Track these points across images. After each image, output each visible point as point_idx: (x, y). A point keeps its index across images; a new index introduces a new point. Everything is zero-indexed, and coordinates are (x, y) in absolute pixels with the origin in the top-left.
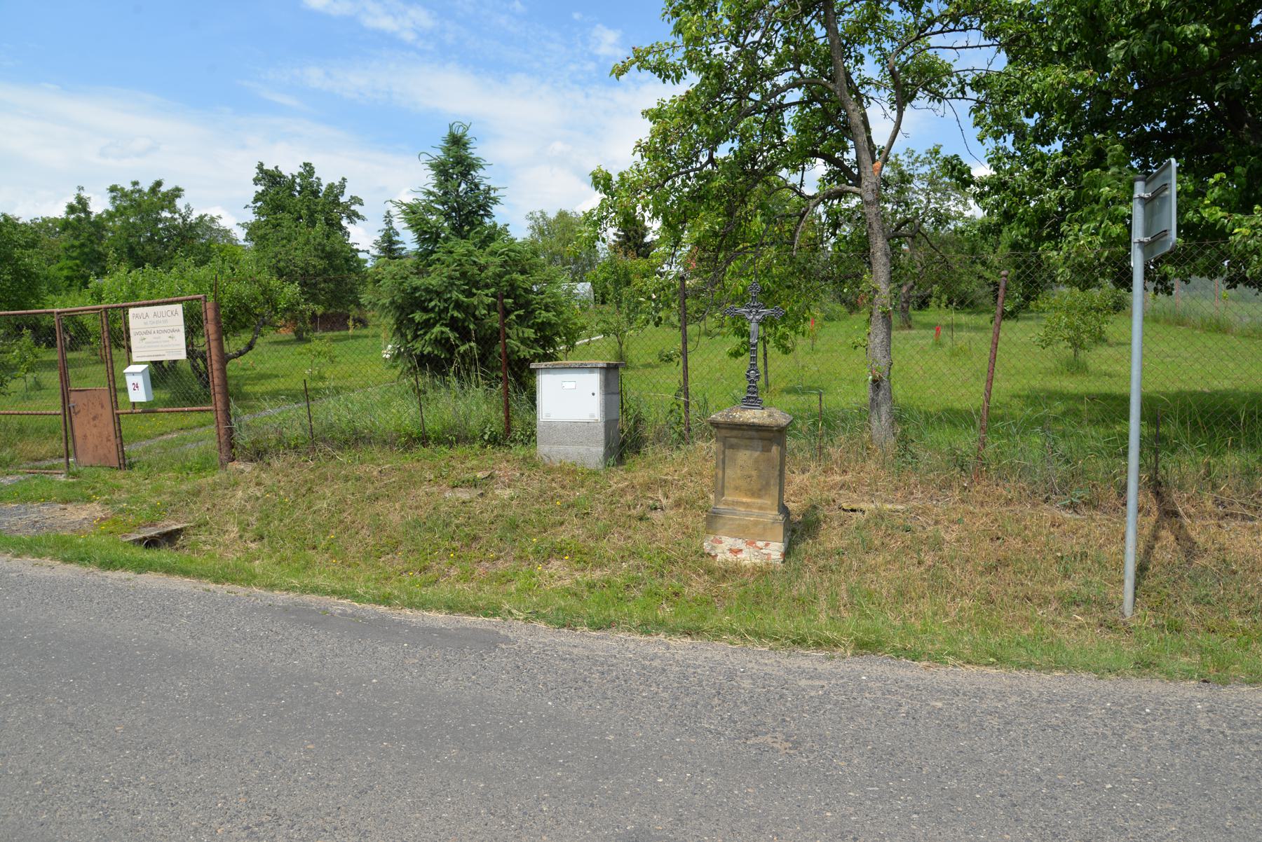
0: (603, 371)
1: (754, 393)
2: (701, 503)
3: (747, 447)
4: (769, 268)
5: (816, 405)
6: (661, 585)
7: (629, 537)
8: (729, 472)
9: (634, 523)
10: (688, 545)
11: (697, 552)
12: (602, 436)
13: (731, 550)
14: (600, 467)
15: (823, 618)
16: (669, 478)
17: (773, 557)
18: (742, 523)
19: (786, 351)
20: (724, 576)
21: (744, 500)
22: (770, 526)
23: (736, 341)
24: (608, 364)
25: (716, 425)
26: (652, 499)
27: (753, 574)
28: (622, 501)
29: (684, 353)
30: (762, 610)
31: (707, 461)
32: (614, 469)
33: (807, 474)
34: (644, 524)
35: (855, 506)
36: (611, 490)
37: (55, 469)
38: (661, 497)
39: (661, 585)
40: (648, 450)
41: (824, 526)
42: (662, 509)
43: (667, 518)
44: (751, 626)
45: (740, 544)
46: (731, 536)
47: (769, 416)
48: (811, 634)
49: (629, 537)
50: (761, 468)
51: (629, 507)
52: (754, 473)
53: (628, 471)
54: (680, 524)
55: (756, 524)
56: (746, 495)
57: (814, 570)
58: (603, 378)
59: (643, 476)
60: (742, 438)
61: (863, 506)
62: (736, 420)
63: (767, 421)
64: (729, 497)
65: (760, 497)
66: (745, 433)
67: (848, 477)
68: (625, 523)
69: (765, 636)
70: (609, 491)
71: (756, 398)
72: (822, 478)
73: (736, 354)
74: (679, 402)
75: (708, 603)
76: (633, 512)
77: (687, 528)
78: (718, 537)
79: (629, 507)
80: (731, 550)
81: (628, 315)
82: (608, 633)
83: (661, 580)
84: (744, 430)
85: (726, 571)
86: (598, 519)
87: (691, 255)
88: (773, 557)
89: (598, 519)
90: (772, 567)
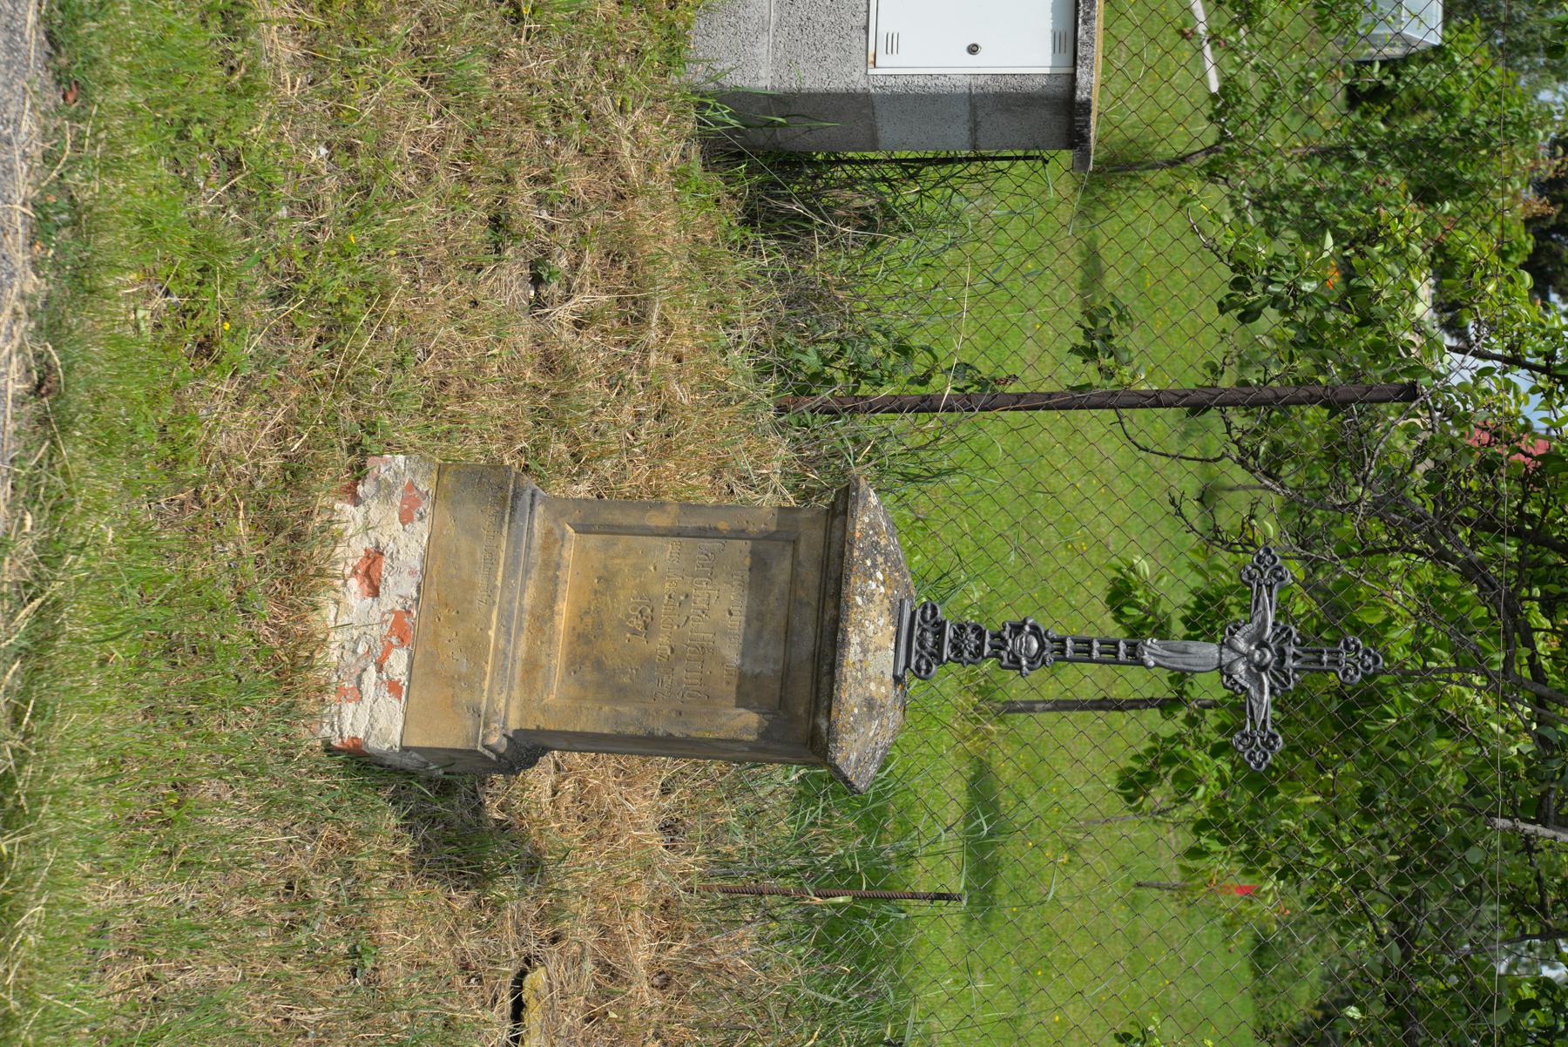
0: (1059, 87)
1: (955, 647)
2: (559, 447)
3: (755, 618)
4: (1449, 726)
5: (922, 877)
6: (242, 293)
7: (427, 176)
8: (666, 552)
9: (482, 197)
10: (398, 397)
11: (370, 428)
12: (812, 79)
14: (697, 74)
15: (105, 897)
16: (653, 334)
17: (349, 708)
19: (1133, 785)
20: (278, 529)
21: (563, 607)
22: (465, 697)
23: (1176, 599)
24: (1086, 107)
25: (842, 506)
26: (575, 266)
27: (284, 634)
28: (568, 153)
29: (1121, 401)
30: (142, 665)
31: (716, 473)
32: (690, 127)
33: (657, 842)
34: (475, 233)
35: (533, 1016)
36: (610, 113)
38: (579, 301)
39: (242, 293)
40: (770, 256)
41: (462, 902)
42: (538, 303)
43: (500, 322)
44: (76, 623)
45: (400, 587)
46: (426, 558)
47: (870, 703)
48: (36, 845)
49: (427, 176)
50: (680, 670)
51: (546, 180)
53: (680, 177)
54: (478, 369)
55: (474, 648)
57: (295, 861)
58: (1029, 86)
59: (660, 235)
62: (856, 581)
63: (850, 696)
64: (572, 548)
65: (574, 663)
66: (809, 614)
67: (643, 990)
68: (483, 161)
69: (32, 676)
70: (605, 105)
71: (937, 656)
72: (640, 897)
73: (1120, 595)
74: (936, 380)
75: (171, 465)
76: (523, 195)
77: (463, 396)
78: (425, 507)
79: (546, 180)
81: (1292, 192)
82: (36, 73)
83: (261, 290)
84: (821, 609)
85: (296, 536)
86: (496, 57)
87: (1507, 432)
89: (496, 57)
90: (309, 705)
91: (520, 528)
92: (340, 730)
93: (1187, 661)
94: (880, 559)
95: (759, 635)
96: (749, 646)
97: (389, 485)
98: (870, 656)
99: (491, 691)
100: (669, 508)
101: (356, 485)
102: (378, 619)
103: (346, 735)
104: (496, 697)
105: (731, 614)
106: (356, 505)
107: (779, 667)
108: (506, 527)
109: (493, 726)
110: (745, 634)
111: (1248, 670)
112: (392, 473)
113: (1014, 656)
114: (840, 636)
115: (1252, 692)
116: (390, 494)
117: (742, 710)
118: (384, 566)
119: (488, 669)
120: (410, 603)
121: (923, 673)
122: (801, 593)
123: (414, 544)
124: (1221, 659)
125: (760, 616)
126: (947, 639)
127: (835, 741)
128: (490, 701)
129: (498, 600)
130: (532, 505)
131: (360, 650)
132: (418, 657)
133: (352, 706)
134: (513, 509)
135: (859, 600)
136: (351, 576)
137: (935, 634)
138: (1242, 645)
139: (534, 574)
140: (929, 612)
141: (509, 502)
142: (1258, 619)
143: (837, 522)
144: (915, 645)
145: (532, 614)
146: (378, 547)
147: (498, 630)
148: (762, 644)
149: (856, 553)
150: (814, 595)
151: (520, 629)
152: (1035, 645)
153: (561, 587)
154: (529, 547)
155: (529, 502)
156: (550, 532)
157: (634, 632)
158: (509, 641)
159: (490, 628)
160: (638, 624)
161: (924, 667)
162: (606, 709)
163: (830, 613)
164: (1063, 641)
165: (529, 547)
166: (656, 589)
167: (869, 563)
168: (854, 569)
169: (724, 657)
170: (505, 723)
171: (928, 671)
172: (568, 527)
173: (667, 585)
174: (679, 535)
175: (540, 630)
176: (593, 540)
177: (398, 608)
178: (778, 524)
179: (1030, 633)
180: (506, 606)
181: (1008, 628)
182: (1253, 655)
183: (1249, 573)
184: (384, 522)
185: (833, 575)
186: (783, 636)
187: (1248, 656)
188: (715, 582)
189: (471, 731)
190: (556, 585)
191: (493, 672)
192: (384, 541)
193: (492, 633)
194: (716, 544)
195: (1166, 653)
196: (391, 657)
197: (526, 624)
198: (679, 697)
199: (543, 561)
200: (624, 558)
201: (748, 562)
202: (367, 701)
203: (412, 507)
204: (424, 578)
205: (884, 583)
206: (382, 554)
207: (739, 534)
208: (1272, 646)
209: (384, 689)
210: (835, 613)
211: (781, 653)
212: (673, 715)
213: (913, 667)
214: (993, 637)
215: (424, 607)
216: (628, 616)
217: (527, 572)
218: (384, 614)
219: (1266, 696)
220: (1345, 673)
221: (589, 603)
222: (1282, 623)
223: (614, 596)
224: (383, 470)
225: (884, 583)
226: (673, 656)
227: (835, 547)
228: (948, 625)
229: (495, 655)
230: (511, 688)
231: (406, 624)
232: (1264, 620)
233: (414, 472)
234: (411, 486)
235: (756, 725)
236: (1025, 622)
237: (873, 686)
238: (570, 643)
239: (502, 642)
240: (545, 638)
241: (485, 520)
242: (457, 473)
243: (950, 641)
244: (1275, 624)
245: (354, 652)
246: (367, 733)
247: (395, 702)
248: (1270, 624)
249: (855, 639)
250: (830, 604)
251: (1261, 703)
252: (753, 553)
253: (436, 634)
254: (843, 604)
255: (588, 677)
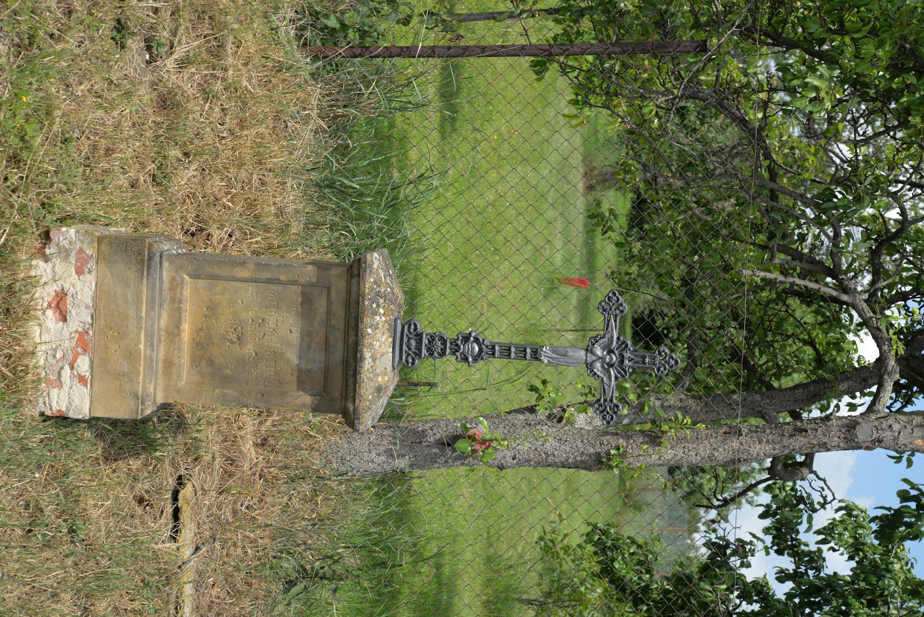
3: (307, 335)
13: (61, 296)
17: (54, 393)
18: (132, 323)
21: (186, 327)
22: (128, 387)
35: (185, 516)
37: (153, 334)
38: (179, 53)
45: (80, 317)
46: (95, 298)
52: (249, 349)
55: (131, 356)
56: (198, 330)
60: (329, 328)
61: (188, 533)
62: (367, 320)
63: (366, 390)
64: (188, 289)
65: (195, 361)
66: (339, 335)
71: (419, 355)
78: (91, 264)
80: (61, 296)
84: (346, 333)
88: (54, 393)
91: (155, 279)
92: (50, 405)
93: (567, 360)
94: (381, 301)
95: (309, 346)
96: (304, 351)
97: (66, 250)
98: (377, 362)
99: (144, 382)
100: (248, 266)
101: (44, 248)
102: (68, 336)
103: (54, 409)
104: (147, 385)
105: (291, 332)
106: (46, 262)
107: (323, 365)
108: (145, 279)
109: (147, 403)
110: (300, 345)
111: (602, 366)
112: (67, 241)
113: (464, 355)
114: (359, 355)
115: (605, 379)
116: (67, 256)
117: (301, 393)
118: (68, 302)
119: (141, 369)
120: (87, 326)
121: (410, 365)
122: (334, 322)
123: (86, 289)
124: (586, 360)
125: (309, 334)
126: (424, 344)
127: (359, 419)
128: (144, 388)
129: (144, 326)
130: (161, 263)
131: (58, 356)
132: (95, 361)
133: (56, 390)
134: (149, 267)
135: (369, 331)
136: (47, 308)
137: (416, 340)
138: (599, 351)
139: (166, 306)
140: (412, 327)
141: (146, 263)
142: (608, 336)
143: (354, 281)
144: (405, 348)
145: (166, 332)
146: (63, 290)
147: (145, 344)
148: (311, 351)
149: (367, 303)
150: (341, 325)
151: (160, 341)
152: (477, 349)
153: (183, 314)
154: (161, 289)
155: (158, 261)
156: (173, 280)
157: (232, 342)
158: (153, 350)
159: (140, 344)
160: (233, 336)
161: (411, 361)
162: (217, 391)
163: (352, 339)
164: (493, 348)
165: (161, 289)
166: (243, 315)
167: (374, 306)
168: (366, 313)
169: (288, 359)
170: (154, 400)
171: (413, 364)
172: (185, 276)
173: (250, 313)
174: (256, 282)
175: (172, 341)
176: (201, 283)
177: (80, 330)
178: (318, 278)
179: (474, 341)
180: (149, 329)
181: (460, 338)
182: (605, 359)
183: (603, 307)
184: (65, 275)
185: (353, 315)
186: (324, 346)
187: (602, 359)
188: (280, 311)
189: (133, 407)
190: (180, 313)
191: (144, 371)
192: (66, 286)
193: (142, 347)
194: (280, 288)
195: (555, 356)
196: (79, 361)
197: (163, 338)
198: (262, 383)
199: (171, 297)
200: (222, 295)
201: (300, 299)
202: (66, 388)
203: (82, 265)
204: (95, 311)
205: (384, 315)
206: (66, 295)
207: (294, 282)
208: (616, 352)
209: (76, 380)
210: (355, 339)
211: (323, 357)
212: (259, 396)
213: (404, 361)
214: (451, 343)
215: (97, 329)
216: (227, 332)
217: (161, 305)
218: (71, 333)
219: (613, 383)
220: (658, 370)
221: (202, 323)
222: (622, 338)
223: (217, 319)
224: (61, 239)
225: (384, 315)
226: (257, 358)
227: (353, 297)
228: (424, 336)
229: (145, 360)
230: (156, 378)
231: (86, 340)
232: (612, 337)
233: (82, 242)
234: (81, 251)
235: (310, 403)
236: (470, 334)
237: (380, 379)
238: (192, 348)
239: (149, 352)
240: (176, 347)
241: (131, 275)
242: (110, 243)
243: (426, 345)
244: (618, 339)
245: (54, 356)
246: (67, 408)
247: (84, 388)
248: (615, 339)
249: (367, 355)
250: (352, 333)
251: (610, 386)
252: (303, 294)
253: (106, 347)
254: (360, 335)
255: (205, 370)
